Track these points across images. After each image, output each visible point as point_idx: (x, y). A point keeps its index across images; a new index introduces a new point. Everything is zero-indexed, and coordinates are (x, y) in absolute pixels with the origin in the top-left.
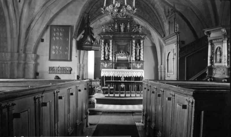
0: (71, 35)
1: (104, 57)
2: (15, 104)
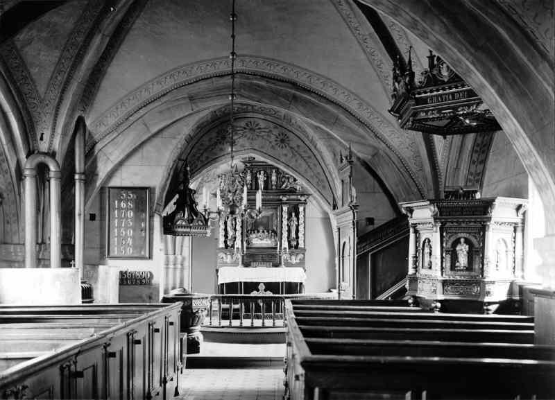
0: (151, 208)
1: (225, 242)
2: (27, 387)
